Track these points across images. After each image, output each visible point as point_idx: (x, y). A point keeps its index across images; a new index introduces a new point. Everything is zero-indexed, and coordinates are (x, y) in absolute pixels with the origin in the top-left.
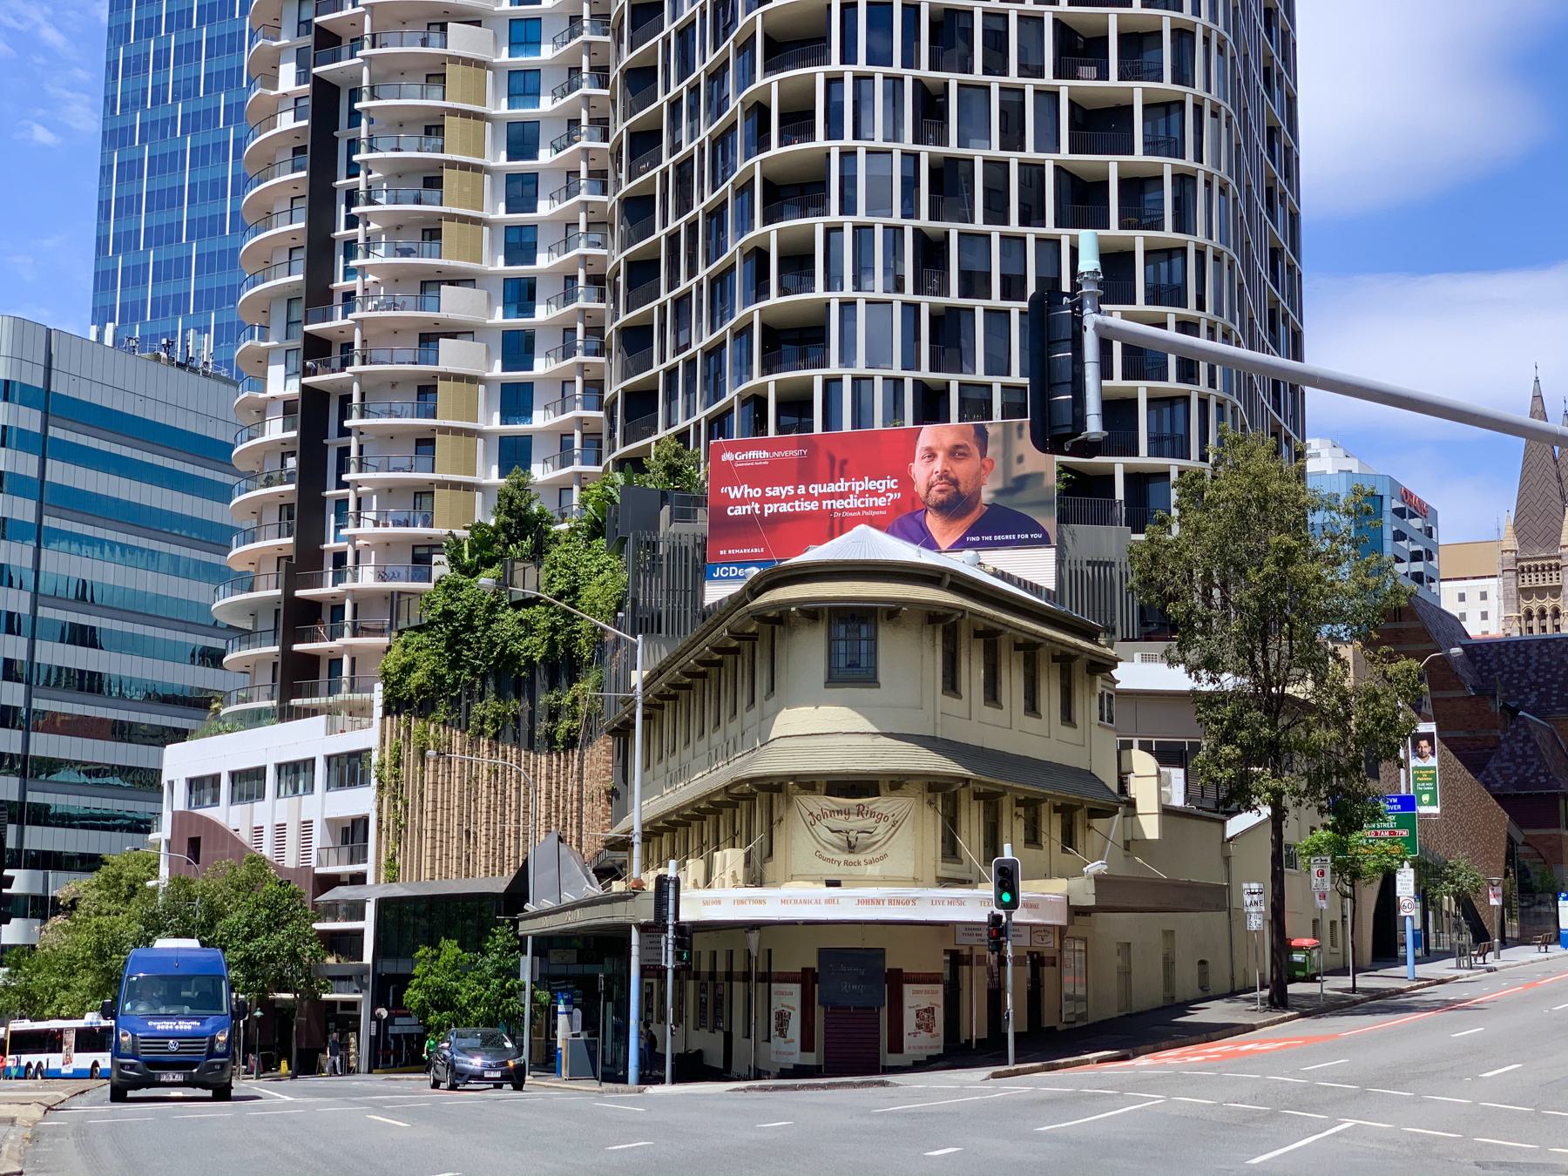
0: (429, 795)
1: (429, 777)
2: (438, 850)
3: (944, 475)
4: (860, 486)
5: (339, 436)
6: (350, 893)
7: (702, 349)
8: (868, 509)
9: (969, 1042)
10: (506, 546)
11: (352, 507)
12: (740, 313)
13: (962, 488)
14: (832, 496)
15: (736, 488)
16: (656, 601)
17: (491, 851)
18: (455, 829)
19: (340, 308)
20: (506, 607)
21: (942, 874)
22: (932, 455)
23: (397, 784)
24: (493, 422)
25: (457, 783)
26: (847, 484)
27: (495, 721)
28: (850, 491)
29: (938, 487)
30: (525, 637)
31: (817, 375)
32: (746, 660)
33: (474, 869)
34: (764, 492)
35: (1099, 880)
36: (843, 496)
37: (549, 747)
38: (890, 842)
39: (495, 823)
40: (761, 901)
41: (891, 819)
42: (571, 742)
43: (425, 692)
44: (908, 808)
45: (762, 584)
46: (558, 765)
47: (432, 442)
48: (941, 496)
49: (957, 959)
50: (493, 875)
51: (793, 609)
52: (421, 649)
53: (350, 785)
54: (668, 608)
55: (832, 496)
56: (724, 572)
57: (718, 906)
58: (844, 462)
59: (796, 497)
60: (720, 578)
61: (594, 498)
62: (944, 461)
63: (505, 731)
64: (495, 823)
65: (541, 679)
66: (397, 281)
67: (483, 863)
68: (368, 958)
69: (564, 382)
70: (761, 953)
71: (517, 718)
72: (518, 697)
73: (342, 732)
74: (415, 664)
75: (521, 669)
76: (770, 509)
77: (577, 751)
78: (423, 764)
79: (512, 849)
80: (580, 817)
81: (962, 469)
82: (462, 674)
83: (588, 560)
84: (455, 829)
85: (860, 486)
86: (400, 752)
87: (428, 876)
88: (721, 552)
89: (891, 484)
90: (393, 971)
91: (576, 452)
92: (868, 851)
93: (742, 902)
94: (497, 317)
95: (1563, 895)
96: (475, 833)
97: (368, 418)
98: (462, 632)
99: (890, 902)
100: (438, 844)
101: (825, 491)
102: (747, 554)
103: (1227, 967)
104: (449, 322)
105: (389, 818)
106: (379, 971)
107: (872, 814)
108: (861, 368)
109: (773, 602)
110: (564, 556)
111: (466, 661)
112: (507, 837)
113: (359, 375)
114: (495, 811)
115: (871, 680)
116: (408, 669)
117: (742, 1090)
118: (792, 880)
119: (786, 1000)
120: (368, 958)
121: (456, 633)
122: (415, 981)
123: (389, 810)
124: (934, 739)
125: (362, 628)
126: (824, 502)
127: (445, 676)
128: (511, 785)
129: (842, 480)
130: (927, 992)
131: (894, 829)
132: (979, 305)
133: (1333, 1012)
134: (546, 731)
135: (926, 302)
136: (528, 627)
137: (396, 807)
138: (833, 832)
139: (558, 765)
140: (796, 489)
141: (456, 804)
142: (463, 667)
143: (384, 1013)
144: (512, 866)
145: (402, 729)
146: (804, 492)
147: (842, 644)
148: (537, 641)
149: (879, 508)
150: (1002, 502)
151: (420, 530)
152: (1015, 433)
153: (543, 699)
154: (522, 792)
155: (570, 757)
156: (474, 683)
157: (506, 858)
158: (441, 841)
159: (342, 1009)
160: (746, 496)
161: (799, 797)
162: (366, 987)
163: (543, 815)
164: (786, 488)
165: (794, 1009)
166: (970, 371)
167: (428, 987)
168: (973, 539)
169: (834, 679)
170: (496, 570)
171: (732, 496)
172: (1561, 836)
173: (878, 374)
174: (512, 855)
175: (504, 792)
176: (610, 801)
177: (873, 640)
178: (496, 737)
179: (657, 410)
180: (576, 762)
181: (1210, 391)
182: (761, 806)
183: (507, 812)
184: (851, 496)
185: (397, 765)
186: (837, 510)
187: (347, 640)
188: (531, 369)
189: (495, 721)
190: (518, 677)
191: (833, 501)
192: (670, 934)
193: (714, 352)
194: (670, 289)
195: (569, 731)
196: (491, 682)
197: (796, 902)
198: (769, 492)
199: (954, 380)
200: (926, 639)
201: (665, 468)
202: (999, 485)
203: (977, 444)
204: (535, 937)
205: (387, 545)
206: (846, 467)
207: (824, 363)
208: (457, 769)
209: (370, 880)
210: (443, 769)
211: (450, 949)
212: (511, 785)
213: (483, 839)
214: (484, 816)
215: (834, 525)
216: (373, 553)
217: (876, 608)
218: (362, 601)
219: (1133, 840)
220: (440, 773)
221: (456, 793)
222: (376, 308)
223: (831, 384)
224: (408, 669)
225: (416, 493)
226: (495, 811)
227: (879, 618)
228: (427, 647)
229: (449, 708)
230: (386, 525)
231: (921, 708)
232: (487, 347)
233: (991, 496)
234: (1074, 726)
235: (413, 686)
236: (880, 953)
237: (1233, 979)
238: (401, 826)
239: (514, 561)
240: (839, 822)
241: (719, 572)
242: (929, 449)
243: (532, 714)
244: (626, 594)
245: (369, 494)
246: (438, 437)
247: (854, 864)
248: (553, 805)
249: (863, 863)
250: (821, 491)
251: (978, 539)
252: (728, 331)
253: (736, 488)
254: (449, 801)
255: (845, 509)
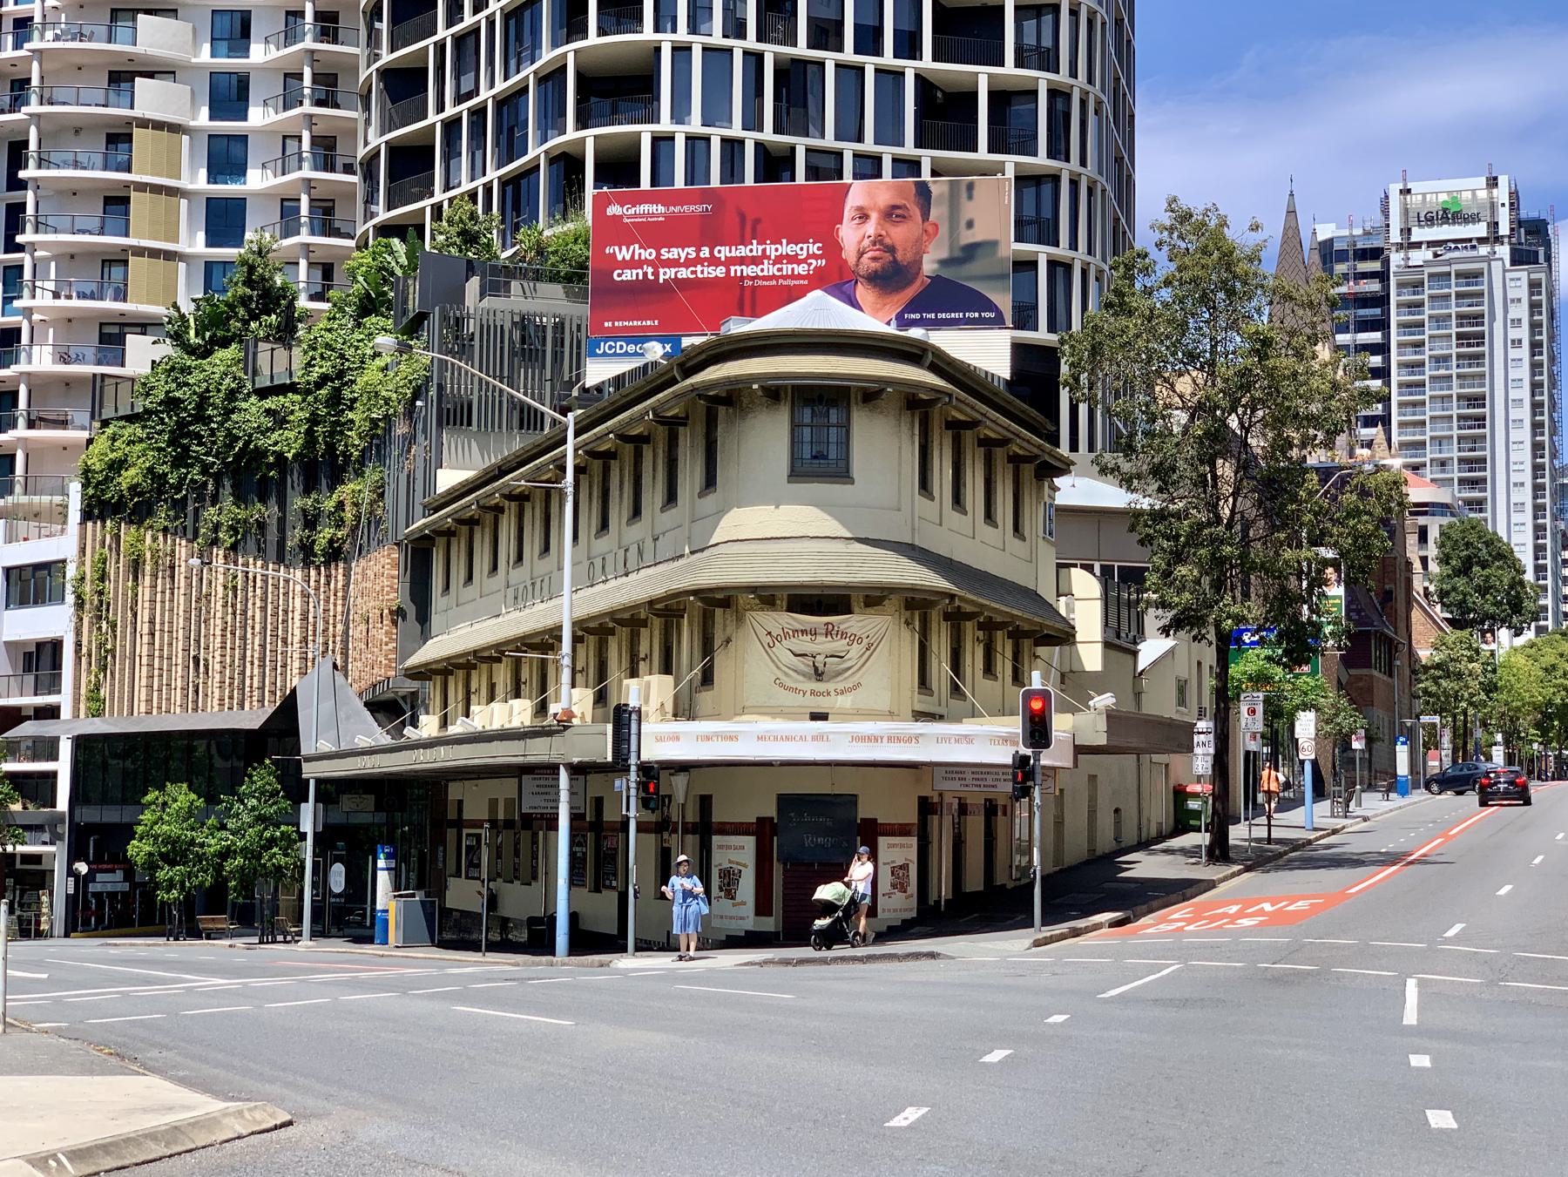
0: (144, 615)
1: (145, 593)
2: (156, 679)
3: (878, 240)
4: (777, 250)
5: (9, 189)
6: (46, 729)
7: (494, 97)
8: (785, 277)
9: (938, 902)
10: (246, 323)
11: (27, 274)
12: (547, 55)
13: (899, 256)
14: (742, 261)
15: (624, 248)
16: (466, 388)
17: (227, 681)
18: (180, 655)
19: (10, 38)
20: (249, 395)
21: (918, 707)
22: (863, 216)
23: (101, 602)
24: (198, 181)
25: (182, 601)
26: (760, 248)
27: (233, 529)
28: (764, 256)
29: (870, 254)
30: (274, 430)
31: (645, 132)
32: (661, 452)
33: (205, 702)
34: (658, 254)
35: (1112, 717)
36: (756, 261)
37: (303, 560)
38: (864, 669)
39: (233, 649)
40: (732, 737)
41: (865, 641)
42: (334, 554)
43: (141, 494)
44: (884, 629)
45: (703, 356)
46: (318, 581)
47: (125, 201)
48: (874, 265)
49: (927, 807)
50: (230, 708)
51: (755, 386)
52: (133, 442)
53: (36, 603)
54: (480, 397)
55: (742, 261)
56: (610, 347)
57: (676, 743)
58: (757, 221)
59: (698, 261)
60: (605, 354)
61: (364, 269)
62: (879, 224)
63: (245, 539)
64: (233, 649)
65: (295, 479)
66: (82, 7)
67: (217, 695)
68: (63, 803)
69: (285, 137)
70: (691, 798)
71: (261, 526)
72: (263, 500)
73: (25, 539)
74: (126, 460)
75: (270, 467)
76: (666, 274)
77: (341, 565)
78: (136, 578)
79: (256, 679)
80: (345, 642)
81: (899, 234)
82: (188, 473)
83: (359, 341)
84: (180, 655)
85: (777, 250)
86: (104, 563)
87: (143, 709)
88: (606, 324)
89: (814, 248)
90: (97, 819)
91: (303, 220)
92: (840, 678)
93: (708, 738)
94: (204, 55)
95: (1402, 739)
96: (206, 660)
97: (48, 168)
98: (191, 423)
99: (890, 739)
100: (156, 672)
101: (733, 254)
102: (637, 327)
103: (1136, 821)
104: (146, 58)
105: (90, 642)
106: (77, 819)
107: (844, 635)
108: (695, 126)
109: (728, 377)
110: (328, 336)
111: (195, 458)
112: (248, 665)
113: (36, 117)
114: (233, 634)
115: (842, 474)
116: (118, 466)
117: (756, 964)
118: (743, 713)
119: (735, 856)
120: (63, 803)
121: (181, 424)
122: (140, 829)
123: (90, 632)
124: (912, 547)
125: (41, 419)
126: (733, 268)
127: (167, 474)
128: (254, 604)
129: (755, 242)
130: (902, 846)
131: (868, 653)
132: (830, 58)
133: (1268, 866)
134: (301, 540)
135: (770, 51)
136: (279, 419)
137: (100, 628)
138: (796, 655)
139: (318, 581)
140: (698, 251)
141: (181, 626)
142: (192, 465)
143: (82, 868)
144: (255, 698)
145: (108, 537)
146: (707, 255)
147: (807, 431)
148: (291, 435)
149: (800, 277)
150: (947, 274)
151: (108, 304)
152: (964, 194)
153: (297, 502)
154: (269, 612)
155: (333, 572)
156: (205, 484)
157: (247, 689)
158: (161, 669)
159: (22, 863)
160: (636, 258)
161: (753, 613)
162: (61, 838)
163: (297, 639)
164: (686, 250)
165: (745, 866)
166: (817, 134)
167: (156, 837)
168: (913, 316)
169: (799, 471)
170: (232, 352)
171: (620, 258)
172: (1372, 676)
173: (716, 134)
174: (256, 685)
175: (244, 612)
176: (395, 623)
177: (846, 427)
178: (234, 547)
179: (433, 168)
180: (340, 577)
181: (1081, 170)
182: (690, 624)
183: (249, 636)
184: (766, 261)
185: (102, 579)
186: (748, 277)
187: (21, 432)
188: (245, 119)
189: (233, 529)
190: (265, 477)
191: (744, 267)
192: (633, 776)
193: (510, 103)
194: (449, 24)
195: (331, 541)
196: (227, 483)
197: (776, 739)
198: (666, 254)
199: (801, 144)
200: (905, 428)
201: (459, 234)
202: (945, 254)
203: (917, 204)
204: (319, 781)
205: (69, 321)
206: (759, 227)
207: (654, 118)
208: (182, 584)
209: (66, 713)
210: (164, 584)
211: (182, 796)
212: (254, 604)
213: (217, 667)
214: (219, 639)
215: (787, 294)
216: (51, 330)
217: (848, 388)
218: (40, 385)
219: (1071, 671)
220: (159, 589)
221: (181, 613)
222: (57, 38)
223: (662, 142)
224: (118, 466)
225: (103, 261)
226: (233, 634)
227: (853, 400)
228: (141, 440)
229: (171, 513)
230: (69, 297)
231: (899, 510)
232: (193, 92)
233: (936, 266)
234: (1024, 539)
235: (124, 486)
236: (852, 800)
237: (1140, 829)
238: (106, 651)
239: (257, 340)
240: (804, 644)
241: (604, 347)
242: (860, 209)
243: (282, 522)
244: (428, 379)
245: (47, 260)
246: (133, 195)
247: (822, 694)
248: (310, 628)
249: (833, 693)
250: (728, 255)
251: (918, 316)
252: (531, 77)
253: (624, 248)
254: (171, 623)
255: (757, 277)
